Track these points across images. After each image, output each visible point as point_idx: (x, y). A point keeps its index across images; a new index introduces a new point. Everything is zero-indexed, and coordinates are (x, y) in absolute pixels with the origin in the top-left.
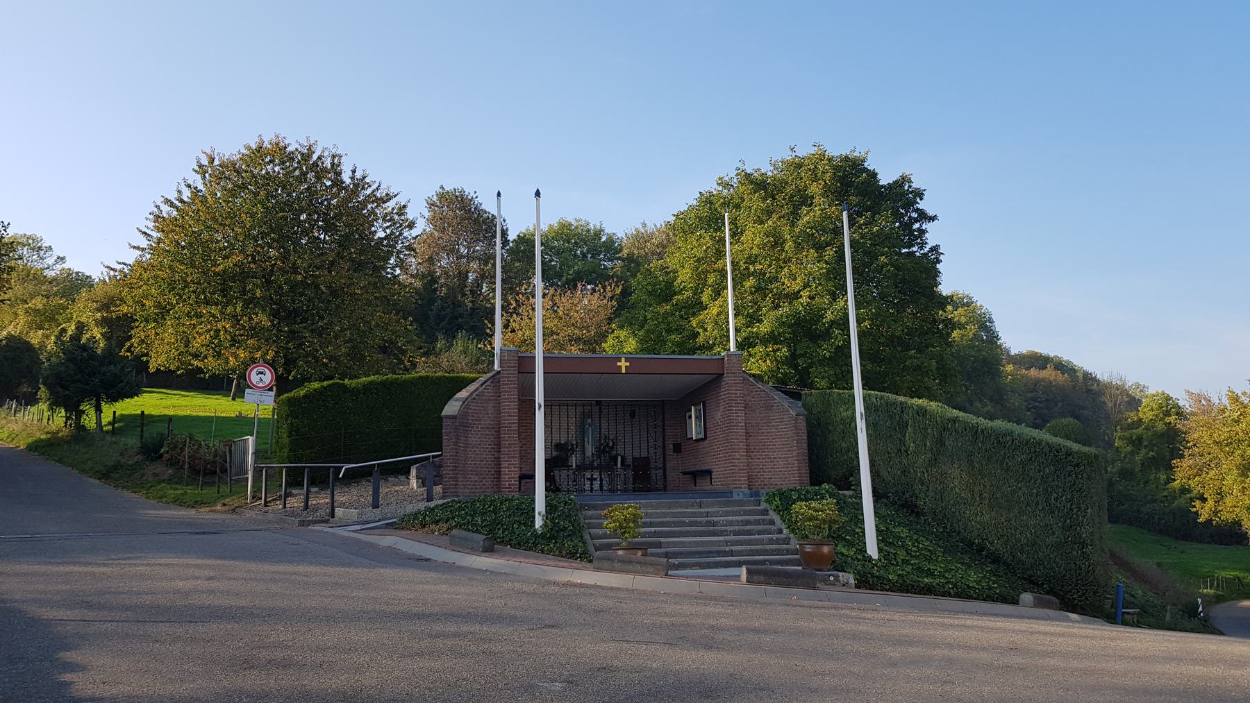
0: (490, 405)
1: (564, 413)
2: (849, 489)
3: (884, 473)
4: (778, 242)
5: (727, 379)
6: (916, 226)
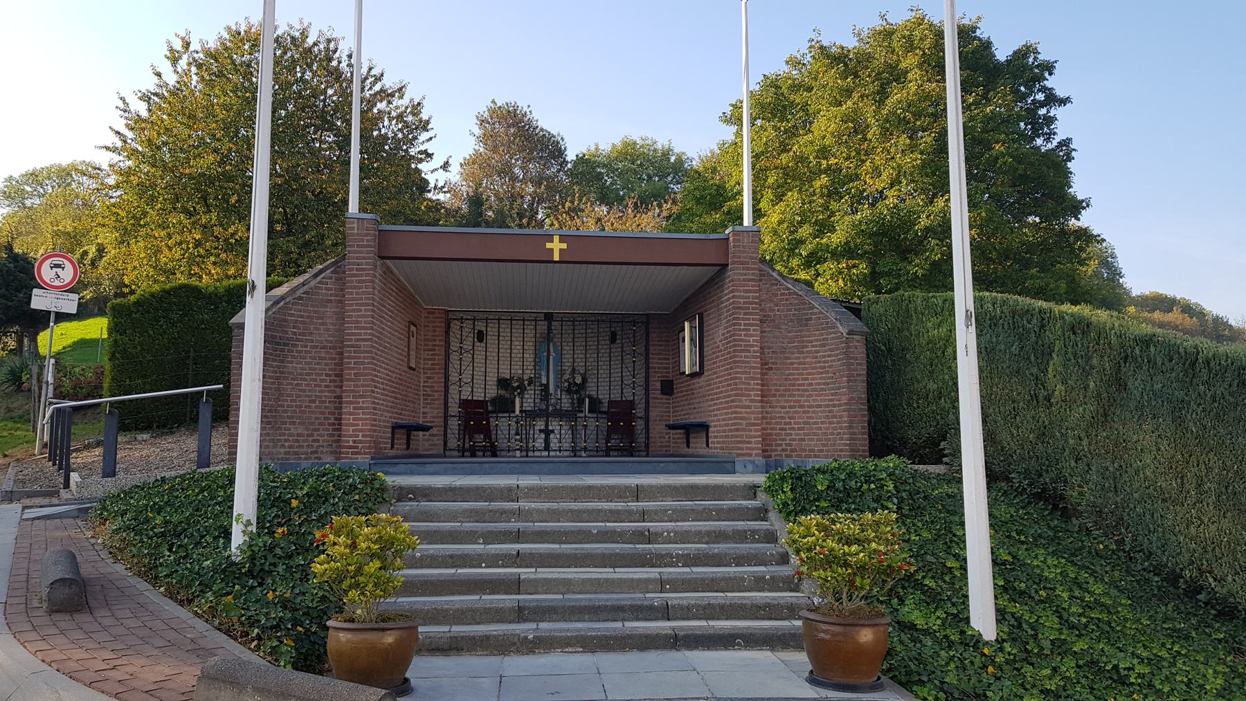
0: (330, 310)
1: (517, 332)
2: (938, 461)
3: (1004, 437)
4: (859, 129)
6: (1043, 111)
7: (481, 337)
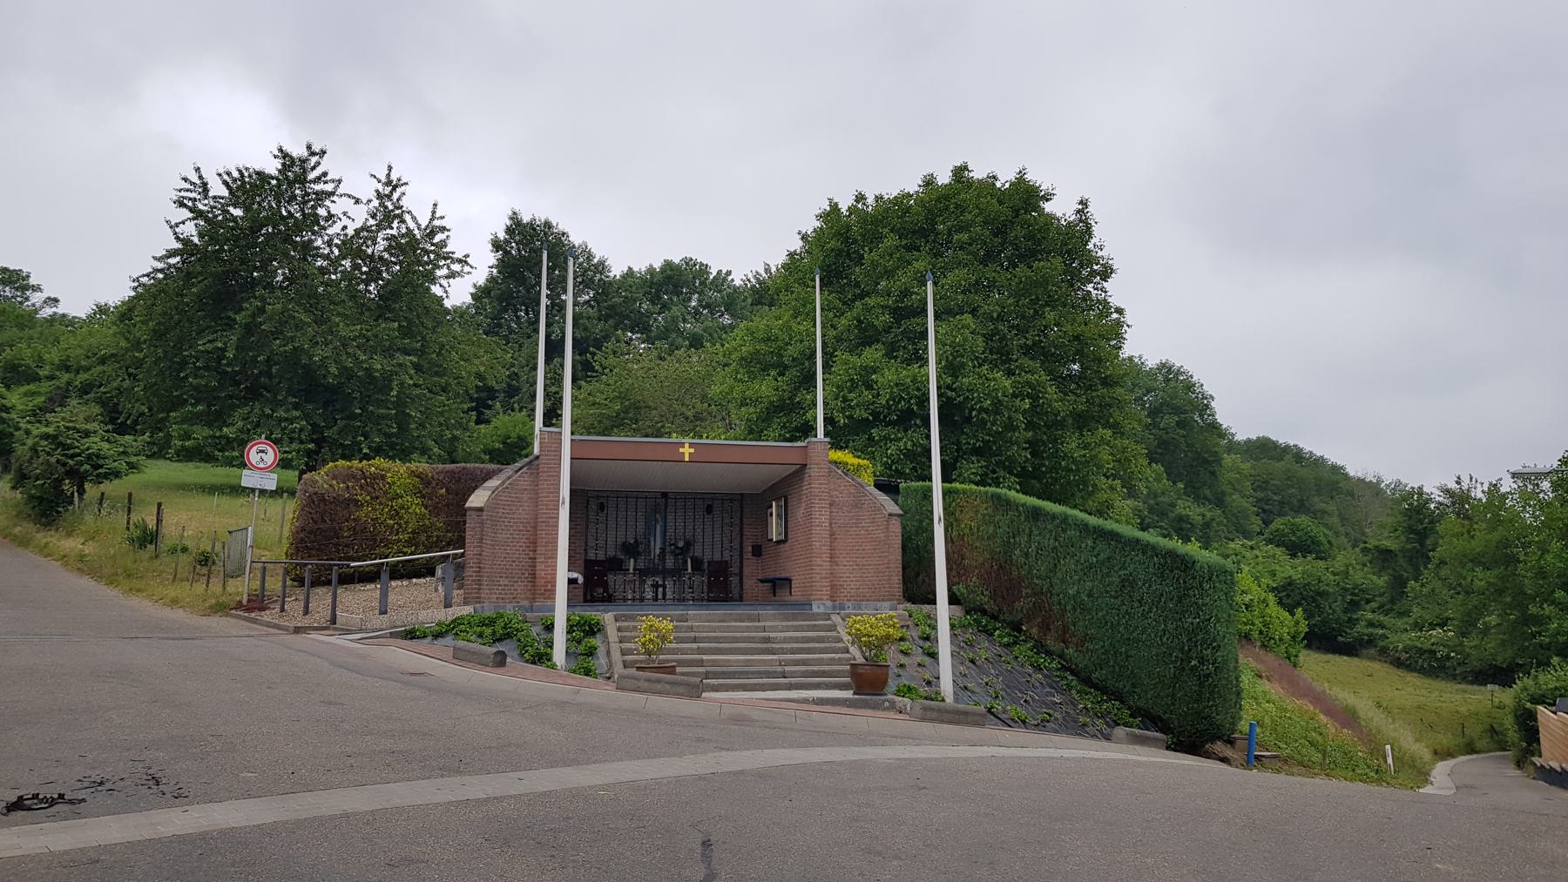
5: (813, 471)
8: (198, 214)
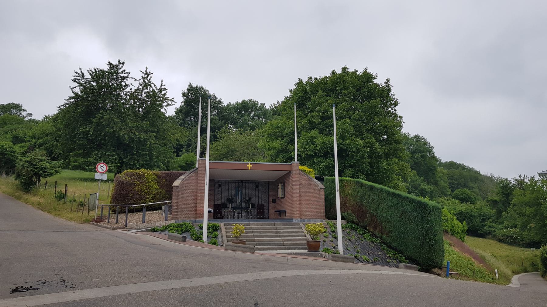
7: (220, 186)
8: (80, 84)
